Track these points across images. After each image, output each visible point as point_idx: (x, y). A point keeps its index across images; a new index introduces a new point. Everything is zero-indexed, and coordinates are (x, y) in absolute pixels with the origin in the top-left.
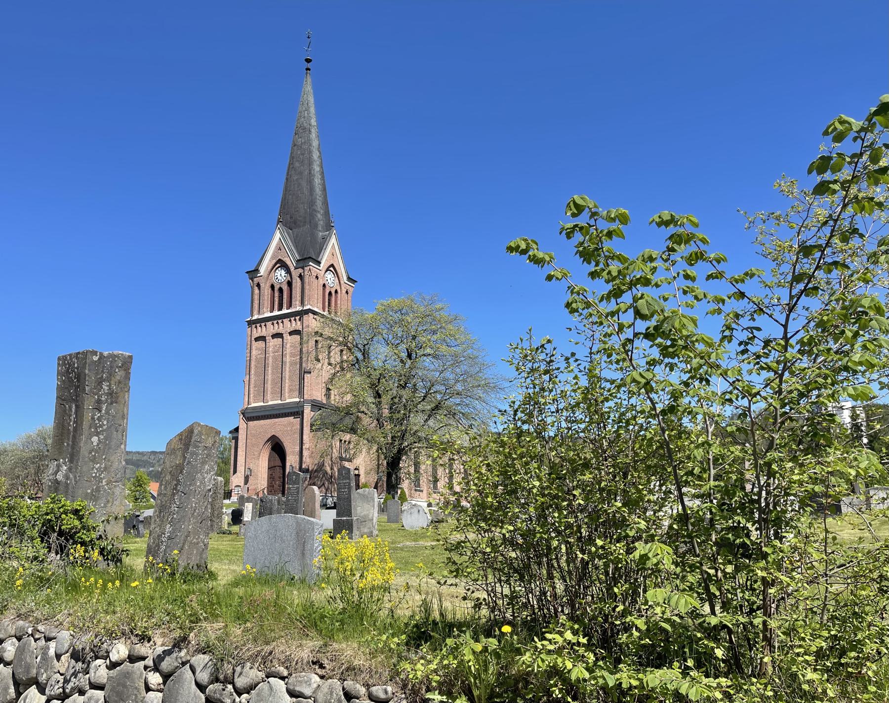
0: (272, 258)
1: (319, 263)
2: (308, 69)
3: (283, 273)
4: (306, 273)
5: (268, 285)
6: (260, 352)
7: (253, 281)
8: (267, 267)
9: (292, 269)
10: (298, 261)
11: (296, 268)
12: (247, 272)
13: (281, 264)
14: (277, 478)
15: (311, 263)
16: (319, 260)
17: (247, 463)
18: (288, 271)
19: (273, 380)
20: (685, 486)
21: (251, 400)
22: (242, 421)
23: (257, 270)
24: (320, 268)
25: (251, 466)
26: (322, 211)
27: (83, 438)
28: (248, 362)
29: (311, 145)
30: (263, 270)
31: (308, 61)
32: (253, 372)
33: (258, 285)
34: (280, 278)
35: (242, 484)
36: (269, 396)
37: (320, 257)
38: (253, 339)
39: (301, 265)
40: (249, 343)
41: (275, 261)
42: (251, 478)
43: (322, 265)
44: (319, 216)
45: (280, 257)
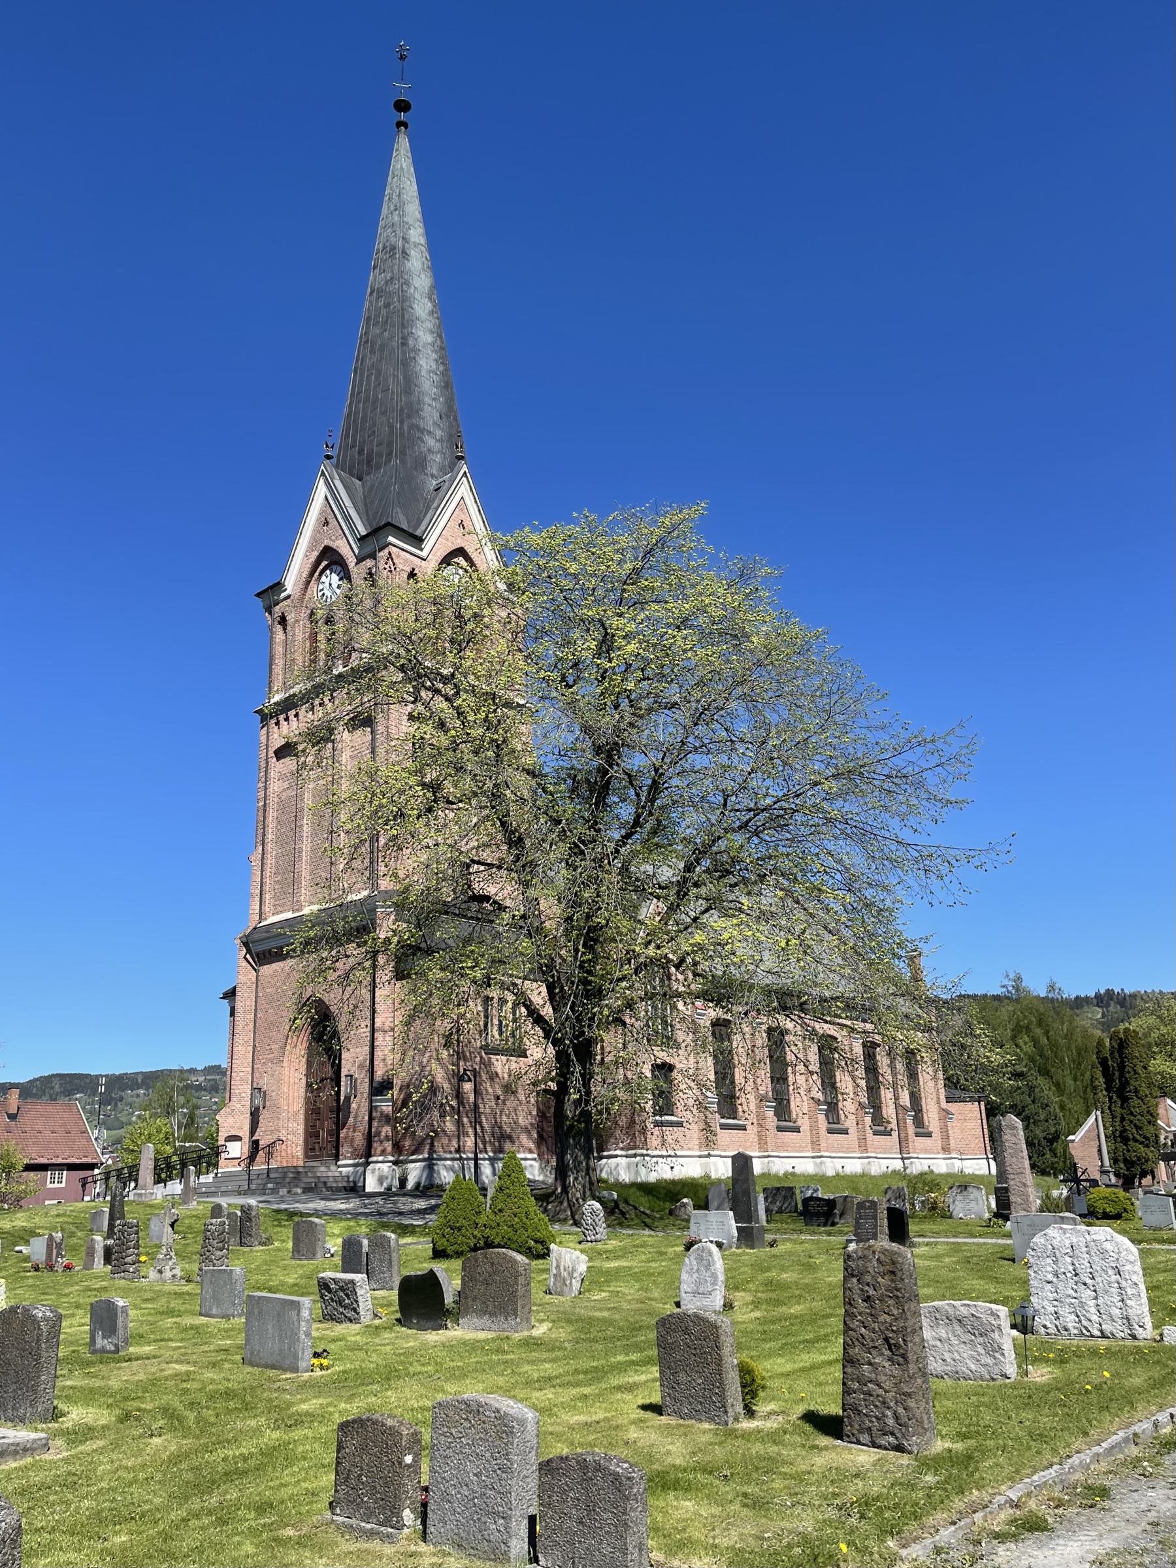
0: (311, 548)
1: (418, 541)
2: (400, 124)
3: (335, 578)
4: (381, 565)
5: (304, 614)
6: (286, 785)
7: (270, 613)
8: (300, 573)
9: (351, 561)
10: (362, 539)
11: (360, 560)
12: (258, 595)
13: (329, 559)
14: (325, 1112)
15: (391, 539)
16: (418, 533)
17: (257, 1075)
18: (346, 575)
19: (314, 850)
20: (519, 1152)
21: (266, 908)
22: (244, 963)
23: (278, 586)
24: (424, 554)
25: (265, 1082)
26: (439, 433)
27: (923, 1101)
28: (261, 813)
29: (407, 283)
30: (291, 583)
31: (402, 106)
32: (270, 836)
33: (283, 621)
34: (328, 593)
35: (245, 1132)
36: (304, 892)
37: (423, 527)
38: (271, 754)
39: (368, 549)
40: (263, 764)
41: (316, 554)
42: (264, 1115)
43: (428, 546)
44: (431, 442)
45: (326, 542)
